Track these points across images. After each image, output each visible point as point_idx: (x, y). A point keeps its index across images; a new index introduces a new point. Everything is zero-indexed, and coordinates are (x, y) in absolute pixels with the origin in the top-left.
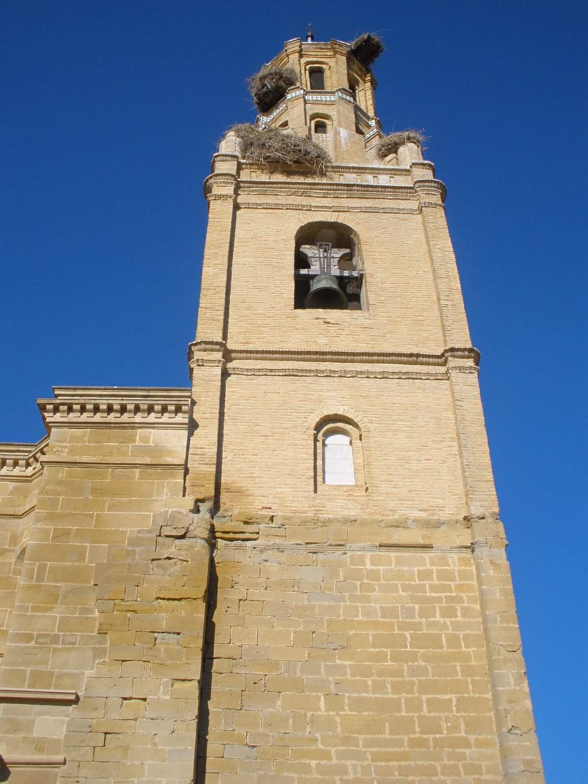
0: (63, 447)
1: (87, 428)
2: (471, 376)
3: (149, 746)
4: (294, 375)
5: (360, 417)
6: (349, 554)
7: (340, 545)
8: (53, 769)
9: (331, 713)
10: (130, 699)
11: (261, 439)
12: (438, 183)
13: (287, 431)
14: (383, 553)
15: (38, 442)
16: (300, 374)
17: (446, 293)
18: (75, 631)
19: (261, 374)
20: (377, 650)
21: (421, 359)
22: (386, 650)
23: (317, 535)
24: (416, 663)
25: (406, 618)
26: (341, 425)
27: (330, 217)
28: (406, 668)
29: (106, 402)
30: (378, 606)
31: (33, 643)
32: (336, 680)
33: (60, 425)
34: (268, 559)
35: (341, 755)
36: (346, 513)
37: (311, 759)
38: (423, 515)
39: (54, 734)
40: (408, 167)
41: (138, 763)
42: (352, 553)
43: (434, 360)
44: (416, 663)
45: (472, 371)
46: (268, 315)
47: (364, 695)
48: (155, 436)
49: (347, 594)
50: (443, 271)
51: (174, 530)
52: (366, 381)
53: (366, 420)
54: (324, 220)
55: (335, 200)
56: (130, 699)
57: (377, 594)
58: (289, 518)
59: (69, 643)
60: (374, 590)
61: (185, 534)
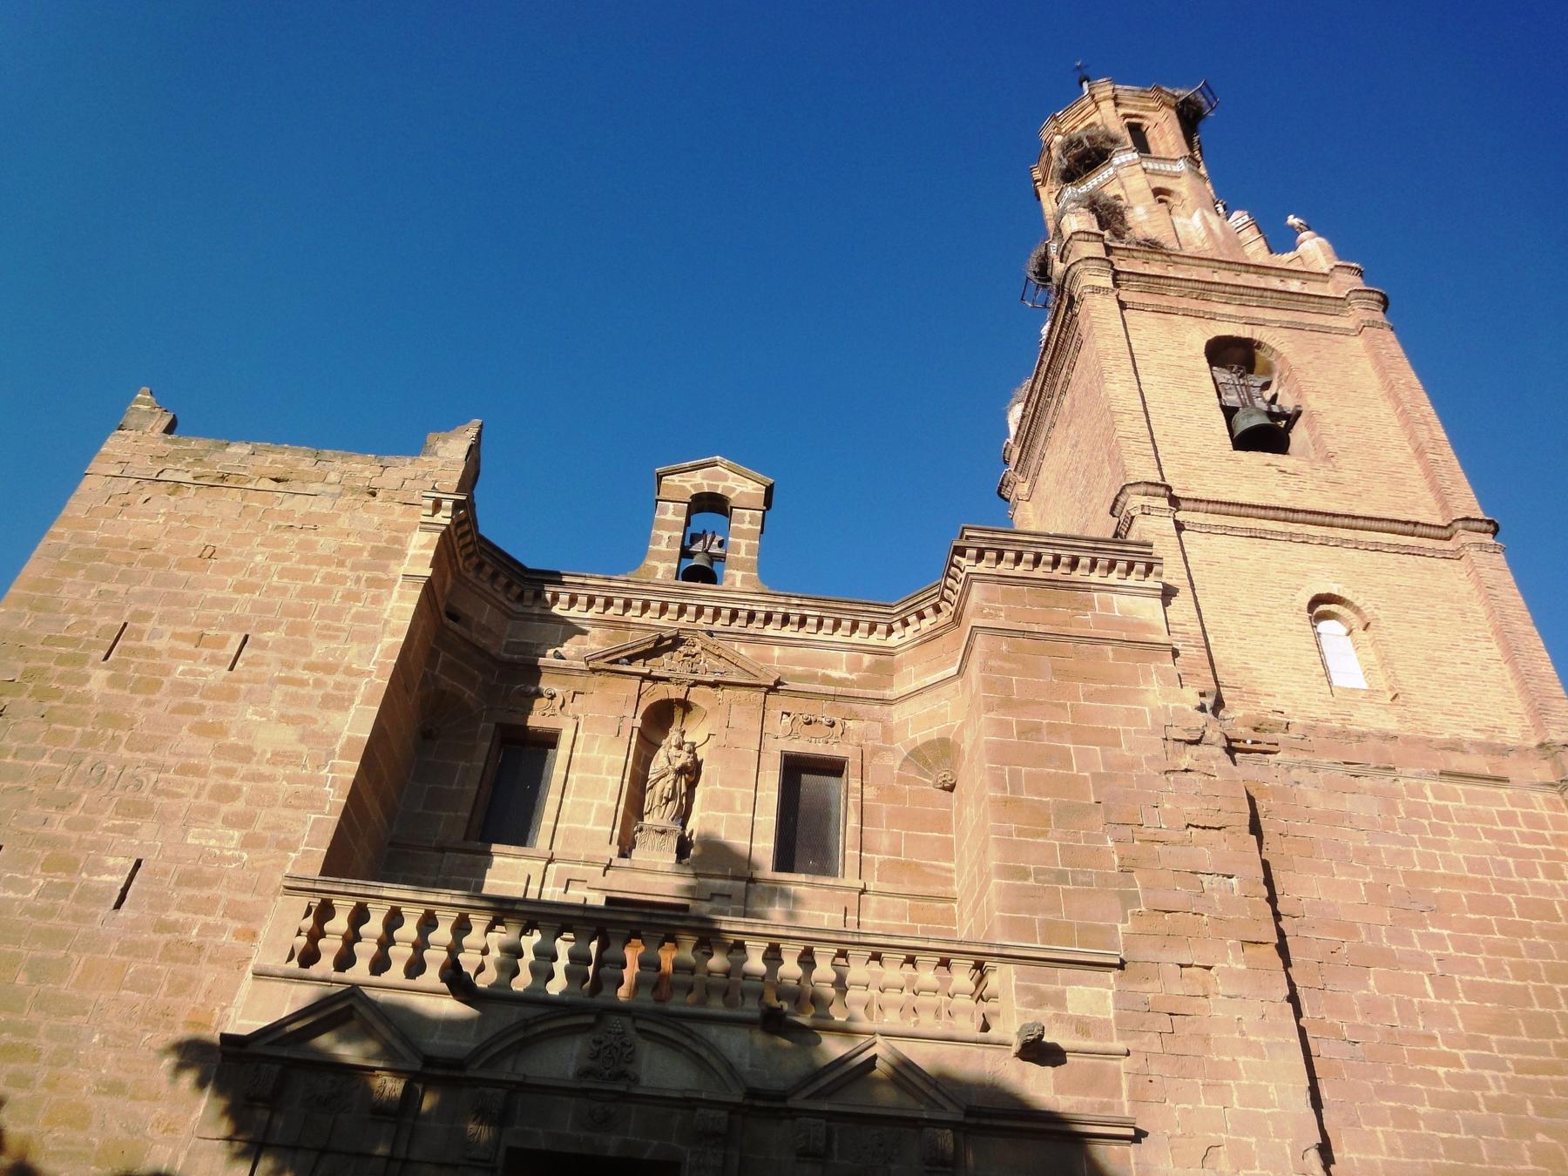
0: (996, 609)
1: (1023, 585)
2: (1496, 557)
3: (1237, 1035)
4: (1261, 538)
5: (1362, 599)
6: (1402, 782)
7: (1390, 768)
8: (1110, 1062)
9: (1444, 1001)
10: (1190, 966)
11: (1245, 619)
12: (1381, 294)
13: (1274, 611)
14: (1447, 785)
15: (897, 602)
16: (1269, 537)
17: (1431, 445)
18: (1087, 867)
19: (1219, 532)
20: (1477, 916)
21: (1419, 529)
22: (1489, 918)
23: (1354, 752)
24: (1533, 939)
25: (1502, 876)
26: (1333, 608)
27: (1244, 332)
28: (1521, 945)
29: (1051, 551)
30: (1461, 856)
31: (1031, 882)
32: (1437, 955)
33: (984, 578)
34: (1300, 780)
35: (1475, 1062)
36: (1380, 725)
37: (1437, 1065)
38: (1481, 737)
39: (1099, 1013)
40: (1326, 271)
41: (1227, 1059)
42: (1406, 781)
43: (1433, 532)
44: (1533, 939)
45: (1497, 550)
46: (1202, 455)
47: (1478, 978)
48: (1120, 602)
49: (1416, 836)
50: (1418, 415)
51: (1186, 734)
52: (1353, 553)
53: (1369, 604)
54: (1235, 334)
55: (1242, 308)
56: (1190, 966)
57: (1453, 839)
58: (1312, 728)
59: (1083, 884)
60: (1448, 834)
61: (1202, 737)
